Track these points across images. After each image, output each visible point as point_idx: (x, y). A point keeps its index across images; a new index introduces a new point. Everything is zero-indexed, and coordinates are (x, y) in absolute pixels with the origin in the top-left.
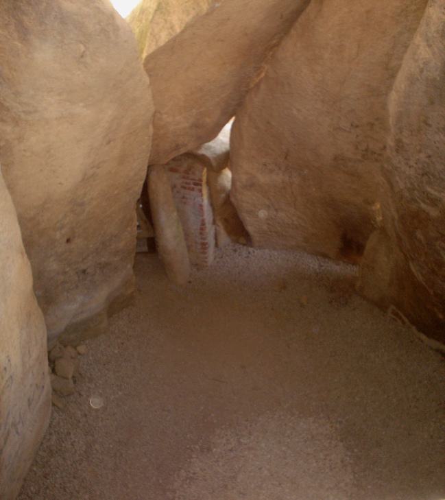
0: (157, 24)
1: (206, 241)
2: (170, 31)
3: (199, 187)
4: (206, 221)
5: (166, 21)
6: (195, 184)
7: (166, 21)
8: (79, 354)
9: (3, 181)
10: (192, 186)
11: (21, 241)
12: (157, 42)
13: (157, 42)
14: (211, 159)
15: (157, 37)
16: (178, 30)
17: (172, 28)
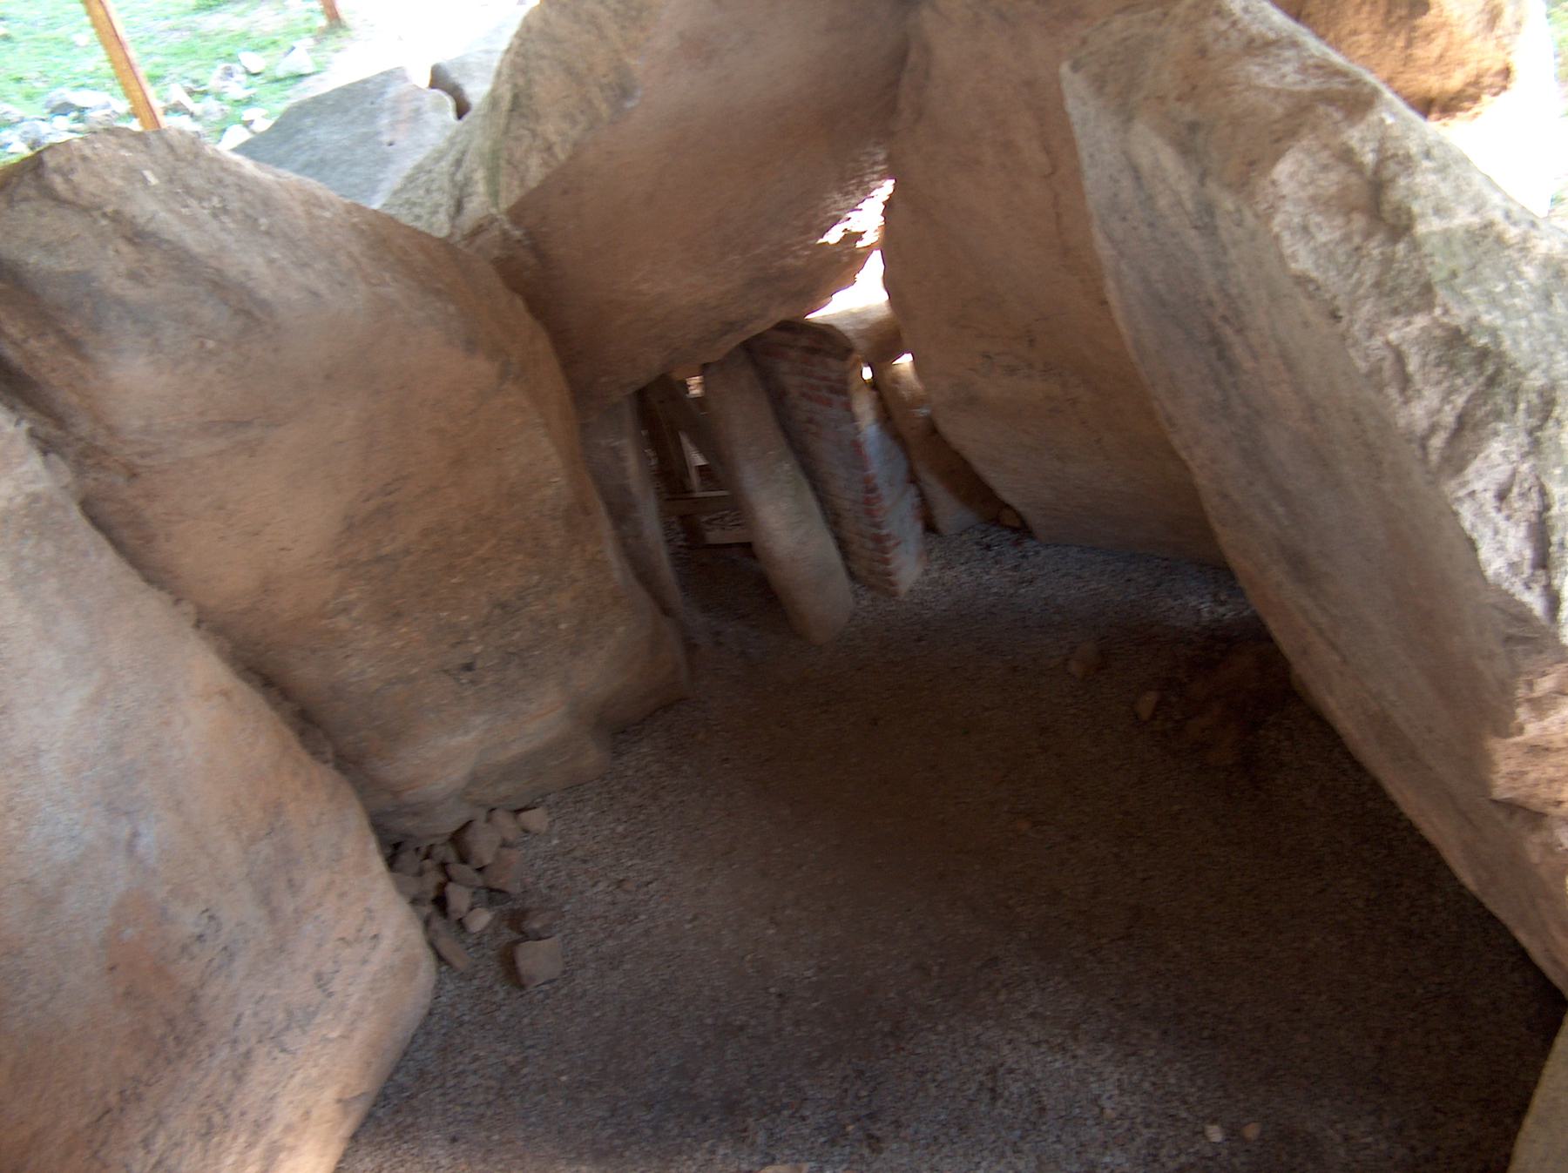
0: (518, 139)
1: (884, 532)
2: (545, 156)
3: (844, 398)
4: (880, 481)
5: (534, 134)
6: (832, 390)
7: (534, 134)
8: (526, 831)
9: (1565, 583)
10: (825, 394)
11: (504, 40)
12: (522, 180)
13: (522, 180)
14: (850, 335)
15: (522, 167)
16: (562, 157)
17: (549, 148)
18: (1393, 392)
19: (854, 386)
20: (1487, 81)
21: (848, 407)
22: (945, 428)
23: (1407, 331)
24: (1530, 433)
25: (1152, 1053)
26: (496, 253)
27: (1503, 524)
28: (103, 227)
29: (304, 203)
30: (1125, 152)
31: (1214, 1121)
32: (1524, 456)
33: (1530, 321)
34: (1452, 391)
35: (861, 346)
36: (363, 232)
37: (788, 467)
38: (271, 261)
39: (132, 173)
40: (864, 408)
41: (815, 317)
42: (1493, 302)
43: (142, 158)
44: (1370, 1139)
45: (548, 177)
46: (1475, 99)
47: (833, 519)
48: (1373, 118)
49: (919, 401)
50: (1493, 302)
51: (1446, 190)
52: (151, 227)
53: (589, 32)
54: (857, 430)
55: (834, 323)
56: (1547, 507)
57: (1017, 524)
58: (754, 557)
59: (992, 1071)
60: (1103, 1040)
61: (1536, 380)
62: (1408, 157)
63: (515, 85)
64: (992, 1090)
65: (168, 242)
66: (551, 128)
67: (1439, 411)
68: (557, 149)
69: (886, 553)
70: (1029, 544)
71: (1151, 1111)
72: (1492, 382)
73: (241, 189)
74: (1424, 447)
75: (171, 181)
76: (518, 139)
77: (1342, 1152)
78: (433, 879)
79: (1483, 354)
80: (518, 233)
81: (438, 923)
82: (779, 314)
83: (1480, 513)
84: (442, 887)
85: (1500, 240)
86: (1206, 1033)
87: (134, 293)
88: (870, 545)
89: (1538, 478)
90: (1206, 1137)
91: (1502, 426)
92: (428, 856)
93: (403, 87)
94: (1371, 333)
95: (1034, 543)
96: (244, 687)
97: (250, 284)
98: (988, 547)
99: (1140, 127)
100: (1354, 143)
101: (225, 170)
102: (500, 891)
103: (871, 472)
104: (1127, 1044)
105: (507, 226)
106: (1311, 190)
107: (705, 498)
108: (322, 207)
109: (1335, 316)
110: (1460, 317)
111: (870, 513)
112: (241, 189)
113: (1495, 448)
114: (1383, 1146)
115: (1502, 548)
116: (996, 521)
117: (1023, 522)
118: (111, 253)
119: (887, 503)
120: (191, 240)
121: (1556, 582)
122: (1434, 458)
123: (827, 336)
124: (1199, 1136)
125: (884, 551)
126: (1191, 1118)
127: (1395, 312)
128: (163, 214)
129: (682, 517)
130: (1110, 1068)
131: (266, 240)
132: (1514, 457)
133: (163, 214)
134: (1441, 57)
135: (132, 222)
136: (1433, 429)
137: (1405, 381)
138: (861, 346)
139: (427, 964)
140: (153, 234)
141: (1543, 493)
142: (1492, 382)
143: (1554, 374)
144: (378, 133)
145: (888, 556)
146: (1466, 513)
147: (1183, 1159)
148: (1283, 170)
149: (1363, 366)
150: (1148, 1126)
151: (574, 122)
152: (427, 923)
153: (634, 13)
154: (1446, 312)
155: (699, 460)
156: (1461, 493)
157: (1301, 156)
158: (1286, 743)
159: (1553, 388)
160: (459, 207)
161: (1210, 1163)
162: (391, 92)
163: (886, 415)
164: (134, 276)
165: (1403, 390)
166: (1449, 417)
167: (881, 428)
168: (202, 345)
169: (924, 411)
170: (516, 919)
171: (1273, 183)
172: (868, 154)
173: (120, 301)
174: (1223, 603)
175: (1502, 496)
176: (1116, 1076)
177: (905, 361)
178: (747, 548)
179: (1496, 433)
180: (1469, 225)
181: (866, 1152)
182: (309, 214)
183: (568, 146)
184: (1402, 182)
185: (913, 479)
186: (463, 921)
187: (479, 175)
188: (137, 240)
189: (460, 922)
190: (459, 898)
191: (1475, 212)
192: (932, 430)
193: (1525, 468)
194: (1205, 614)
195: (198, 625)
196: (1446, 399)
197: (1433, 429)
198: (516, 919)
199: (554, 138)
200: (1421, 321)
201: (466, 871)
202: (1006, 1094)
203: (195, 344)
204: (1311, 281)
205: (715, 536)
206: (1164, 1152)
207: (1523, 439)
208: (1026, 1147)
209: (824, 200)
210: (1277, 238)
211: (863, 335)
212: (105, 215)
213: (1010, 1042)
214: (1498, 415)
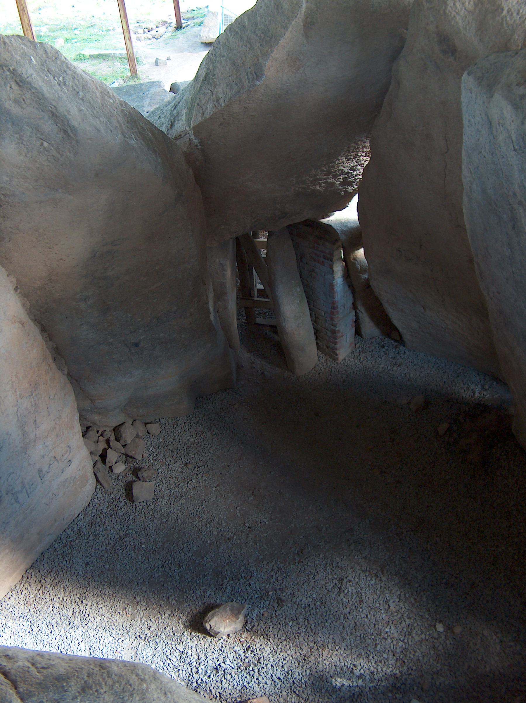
6: (325, 258)
13: (203, 114)
19: (335, 258)
21: (331, 267)
22: (373, 283)
25: (417, 585)
26: (185, 149)
28: (7, 75)
29: (101, 92)
30: (486, 115)
31: (440, 622)
35: (343, 237)
36: (126, 115)
37: (299, 290)
38: (80, 110)
39: (25, 55)
40: (338, 269)
41: (325, 221)
43: (31, 52)
44: (512, 644)
45: (215, 114)
47: (315, 319)
49: (363, 271)
52: (29, 79)
53: (246, 46)
54: (333, 278)
55: (333, 225)
57: (398, 339)
58: (276, 333)
59: (341, 580)
60: (396, 575)
63: (208, 69)
64: (340, 588)
65: (36, 88)
66: (220, 91)
68: (222, 101)
69: (336, 339)
70: (401, 348)
71: (412, 611)
73: (74, 78)
75: (43, 65)
76: (204, 94)
77: (498, 647)
78: (102, 445)
80: (196, 142)
81: (100, 465)
82: (307, 215)
84: (105, 451)
86: (444, 581)
87: (15, 110)
88: (329, 334)
90: (435, 628)
92: (102, 435)
93: (158, 89)
95: (404, 348)
96: (32, 323)
97: (69, 117)
98: (383, 347)
99: (498, 97)
101: (67, 67)
102: (131, 457)
103: (336, 299)
104: (407, 579)
105: (192, 137)
107: (258, 300)
108: (109, 97)
111: (332, 319)
112: (74, 78)
114: (518, 648)
116: (389, 335)
117: (401, 337)
118: (8, 88)
119: (341, 316)
120: (45, 90)
124: (433, 628)
125: (336, 338)
126: (430, 618)
128: (35, 76)
129: (246, 308)
130: (397, 588)
131: (81, 102)
133: (35, 76)
135: (20, 76)
138: (343, 237)
139: (92, 480)
140: (29, 83)
144: (143, 106)
147: (423, 636)
150: (409, 618)
151: (231, 89)
152: (95, 464)
153: (268, 39)
155: (260, 287)
158: (504, 457)
160: (172, 125)
161: (436, 641)
162: (152, 90)
163: (348, 275)
164: (16, 101)
167: (344, 280)
168: (42, 144)
170: (136, 472)
172: (362, 141)
173: (8, 112)
174: (486, 390)
176: (399, 593)
177: (361, 253)
178: (274, 328)
181: (276, 605)
182: (103, 97)
183: (226, 100)
185: (354, 306)
186: (112, 467)
187: (184, 112)
188: (21, 84)
189: (110, 467)
190: (112, 456)
192: (368, 286)
194: (477, 394)
195: (16, 289)
198: (136, 472)
199: (221, 95)
201: (118, 445)
202: (346, 591)
203: (39, 143)
205: (259, 320)
206: (414, 631)
208: (350, 617)
209: (339, 160)
211: (344, 232)
212: (9, 70)
213: (352, 568)
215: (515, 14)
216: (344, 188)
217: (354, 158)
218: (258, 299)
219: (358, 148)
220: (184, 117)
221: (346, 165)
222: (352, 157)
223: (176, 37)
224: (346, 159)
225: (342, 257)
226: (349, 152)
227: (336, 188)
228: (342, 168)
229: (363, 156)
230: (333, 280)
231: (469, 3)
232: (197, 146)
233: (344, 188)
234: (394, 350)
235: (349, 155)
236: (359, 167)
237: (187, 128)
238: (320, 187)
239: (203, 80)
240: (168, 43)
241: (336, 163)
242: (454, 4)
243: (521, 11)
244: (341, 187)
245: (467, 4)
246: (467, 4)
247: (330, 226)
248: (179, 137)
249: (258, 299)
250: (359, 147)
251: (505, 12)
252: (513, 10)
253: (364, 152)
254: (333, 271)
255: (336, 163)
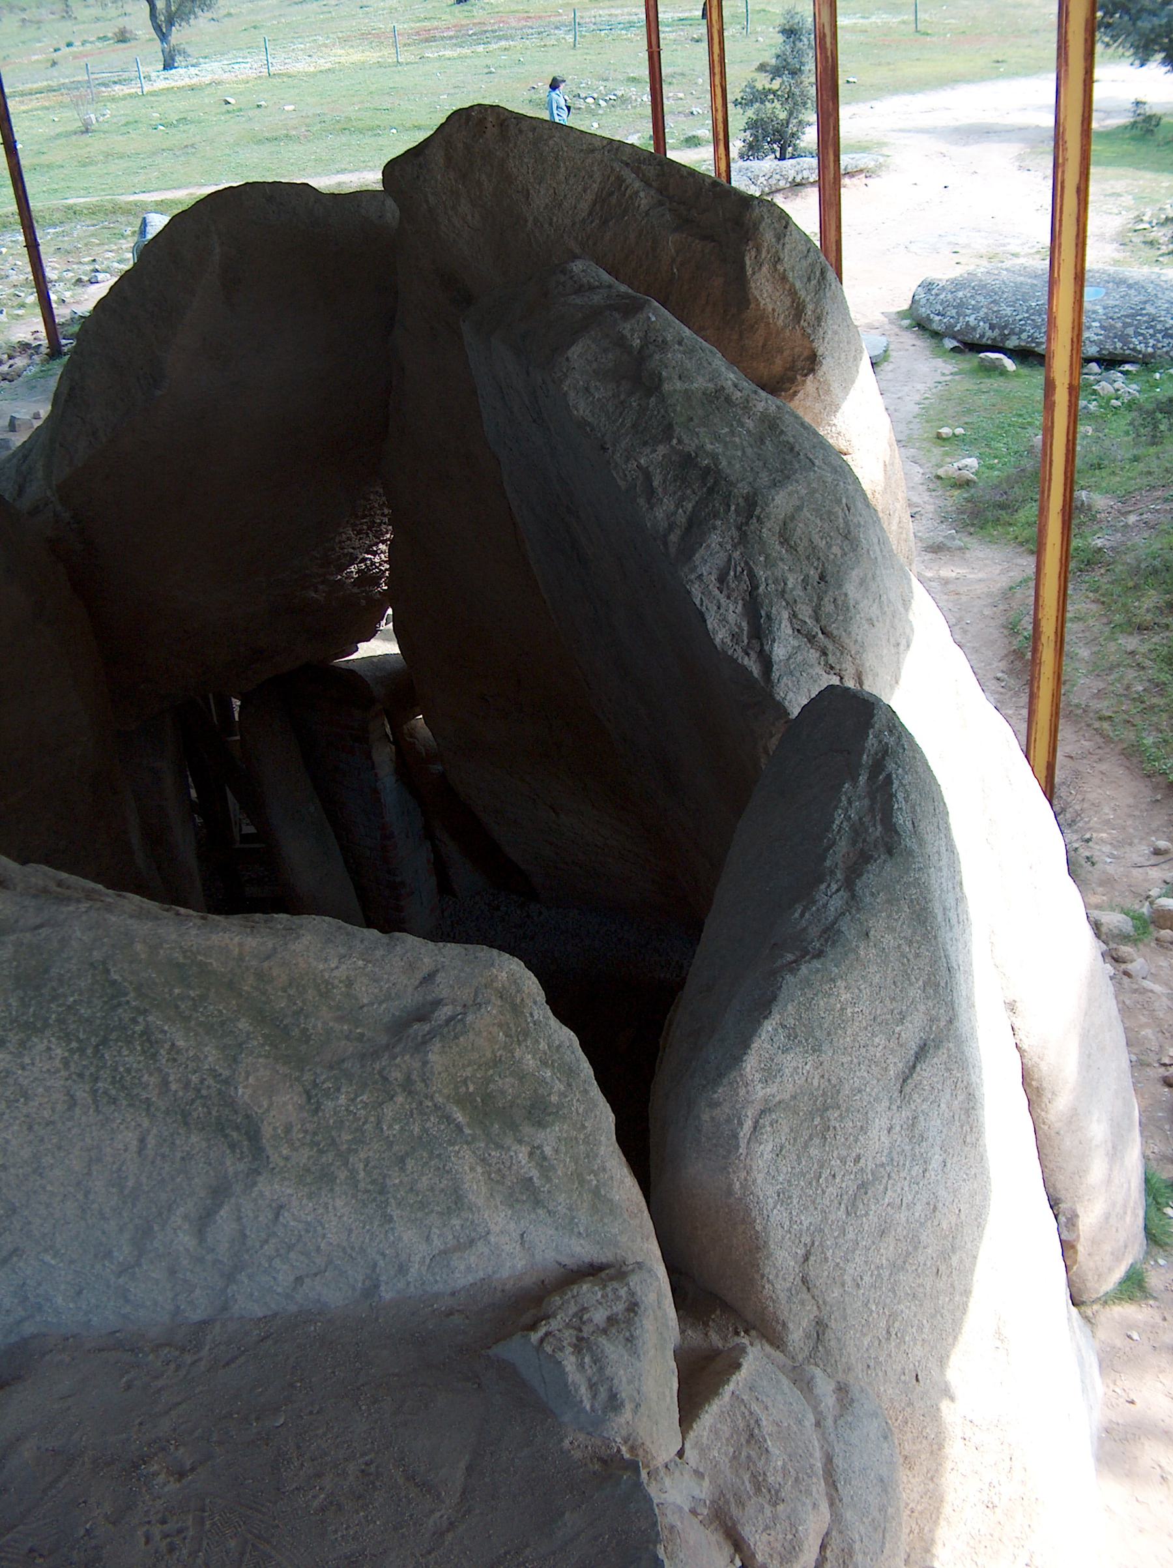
1: (398, 879)
18: (642, 501)
20: (799, 364)
21: (369, 756)
23: (654, 457)
24: (739, 528)
27: (723, 600)
32: (735, 546)
33: (744, 452)
34: (683, 498)
40: (384, 756)
42: (717, 438)
46: (792, 380)
48: (641, 316)
50: (717, 438)
51: (688, 364)
55: (356, 669)
56: (755, 587)
61: (743, 488)
62: (664, 342)
67: (674, 513)
72: (711, 491)
74: (665, 544)
79: (707, 471)
83: (706, 592)
85: (728, 399)
89: (747, 563)
91: (719, 523)
94: (628, 460)
98: (498, 908)
100: (626, 333)
105: (59, 508)
106: (595, 365)
109: (604, 449)
110: (690, 446)
113: (714, 539)
115: (724, 620)
121: (767, 648)
122: (673, 550)
123: (352, 678)
127: (645, 444)
132: (729, 547)
134: (764, 346)
136: (671, 527)
137: (650, 492)
141: (752, 576)
142: (711, 491)
143: (756, 486)
145: (402, 903)
146: (696, 591)
148: (575, 352)
149: (622, 484)
154: (680, 441)
156: (693, 577)
157: (589, 342)
159: (755, 494)
160: (21, 491)
165: (649, 501)
166: (681, 519)
169: (437, 768)
171: (567, 359)
175: (722, 579)
179: (715, 528)
180: (706, 389)
184: (657, 357)
191: (711, 380)
193: (736, 555)
196: (679, 505)
197: (671, 527)
200: (662, 449)
204: (589, 424)
207: (734, 532)
210: (565, 394)
214: (716, 515)
215: (546, 226)
216: (363, 591)
217: (368, 529)
218: (242, 846)
219: (371, 509)
220: (40, 474)
221: (357, 544)
222: (365, 527)
223: (50, 373)
224: (353, 530)
225: (387, 735)
226: (357, 516)
227: (348, 592)
228: (352, 551)
229: (385, 524)
230: (376, 781)
231: (473, 216)
232: (69, 523)
233: (363, 591)
234: (519, 912)
235: (358, 522)
236: (381, 546)
237: (49, 493)
238: (316, 592)
239: (66, 401)
240: (35, 387)
241: (337, 541)
242: (449, 220)
243: (555, 219)
244: (356, 590)
245: (469, 217)
246: (469, 217)
247: (351, 672)
248: (35, 511)
249: (242, 846)
250: (374, 507)
251: (530, 224)
252: (541, 219)
253: (385, 516)
254: (373, 763)
255: (337, 541)
